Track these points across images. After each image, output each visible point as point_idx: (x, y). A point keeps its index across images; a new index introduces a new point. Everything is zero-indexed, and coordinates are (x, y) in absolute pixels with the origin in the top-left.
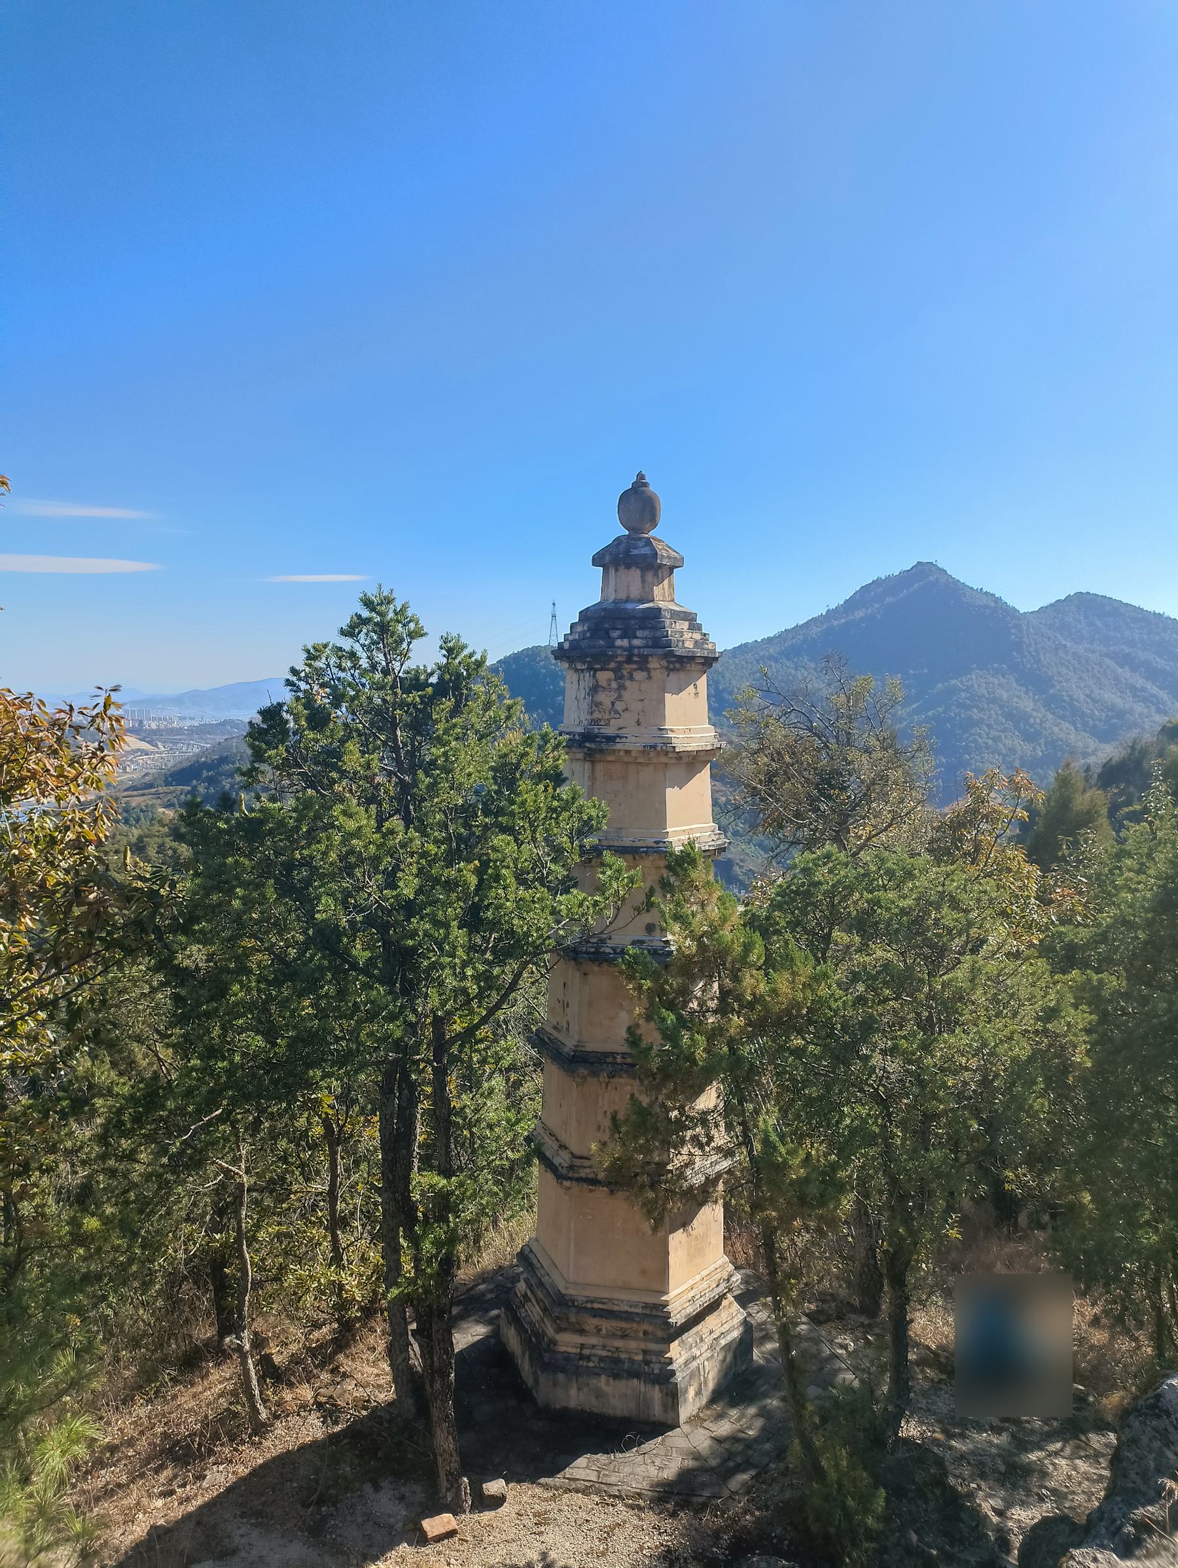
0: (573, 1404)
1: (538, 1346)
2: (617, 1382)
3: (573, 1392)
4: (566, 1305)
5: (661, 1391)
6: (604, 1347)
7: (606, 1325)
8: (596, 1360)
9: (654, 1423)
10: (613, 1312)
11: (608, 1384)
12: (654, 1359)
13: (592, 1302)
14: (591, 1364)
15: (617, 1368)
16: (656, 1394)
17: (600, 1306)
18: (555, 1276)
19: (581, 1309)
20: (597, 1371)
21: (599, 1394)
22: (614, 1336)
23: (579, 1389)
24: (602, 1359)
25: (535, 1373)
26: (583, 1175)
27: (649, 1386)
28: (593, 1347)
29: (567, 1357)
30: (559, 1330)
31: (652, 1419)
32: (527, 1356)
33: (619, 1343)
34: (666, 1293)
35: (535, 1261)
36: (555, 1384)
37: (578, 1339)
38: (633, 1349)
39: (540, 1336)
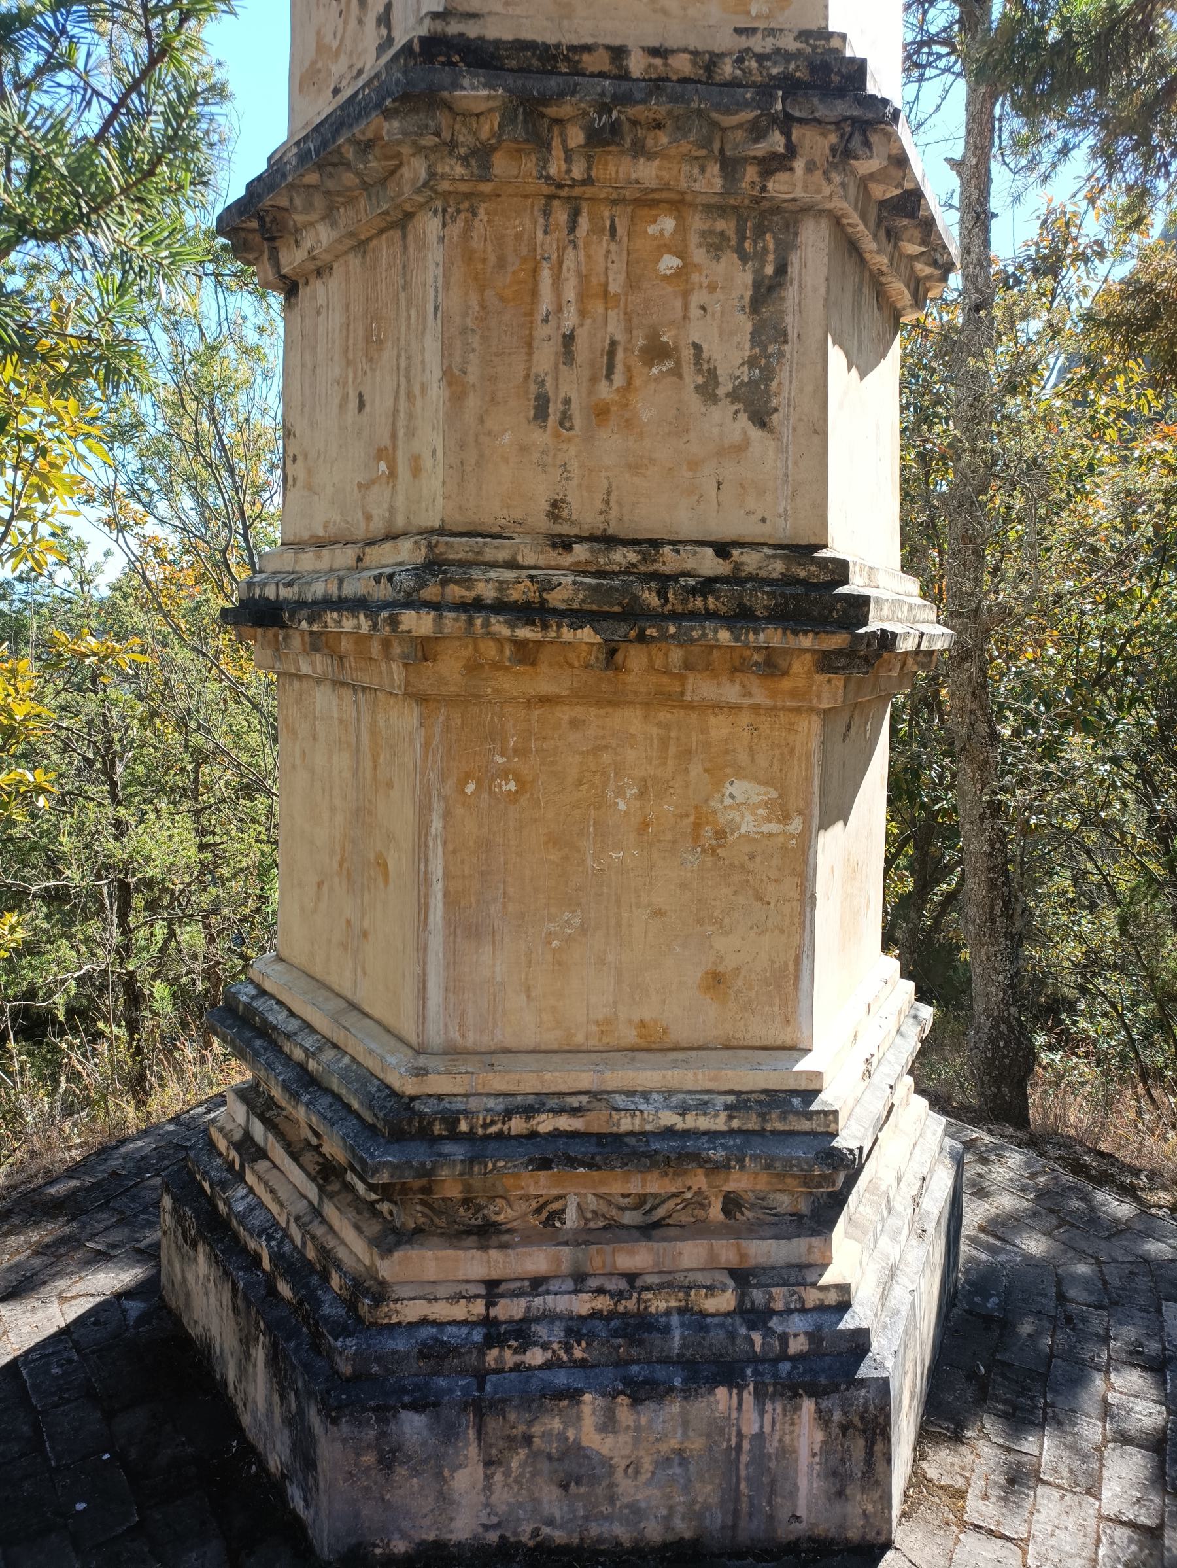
0: (463, 1527)
1: (306, 1315)
2: (647, 1414)
3: (466, 1479)
4: (424, 1134)
5: (823, 1418)
6: (579, 1280)
7: (579, 1195)
8: (555, 1334)
9: (793, 1547)
10: (617, 1138)
11: (609, 1425)
12: (780, 1298)
13: (529, 1111)
14: (536, 1357)
15: (639, 1355)
16: (804, 1432)
17: (565, 1123)
18: (365, 1047)
19: (484, 1145)
20: (561, 1378)
21: (575, 1470)
22: (612, 1231)
23: (488, 1463)
24: (576, 1329)
25: (296, 1423)
26: (489, 593)
27: (775, 1408)
28: (537, 1284)
29: (436, 1348)
30: (391, 1238)
31: (786, 1532)
32: (260, 1355)
33: (637, 1257)
34: (800, 1050)
35: (277, 1018)
36: (389, 1458)
37: (475, 1264)
38: (691, 1267)
39: (307, 1272)
